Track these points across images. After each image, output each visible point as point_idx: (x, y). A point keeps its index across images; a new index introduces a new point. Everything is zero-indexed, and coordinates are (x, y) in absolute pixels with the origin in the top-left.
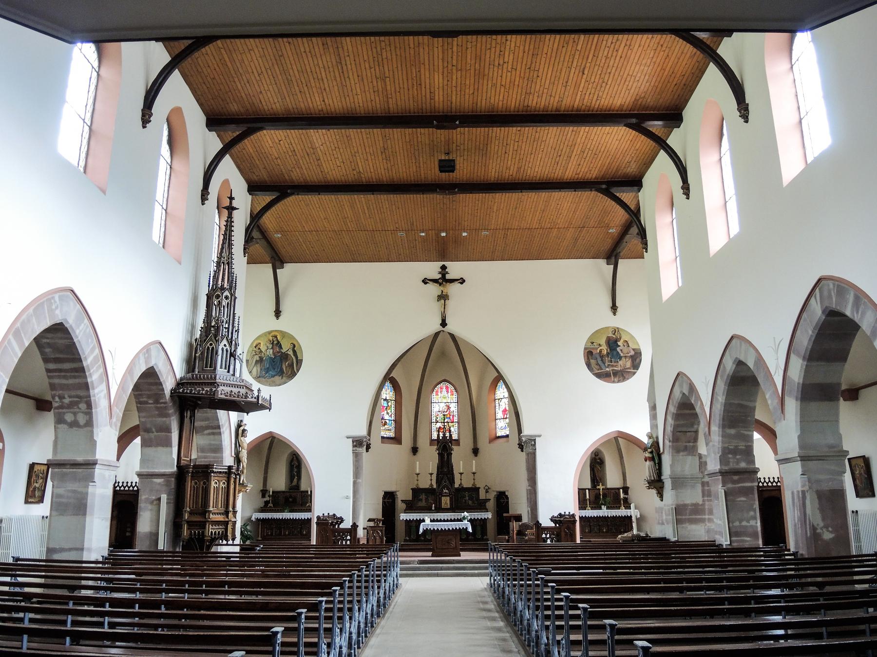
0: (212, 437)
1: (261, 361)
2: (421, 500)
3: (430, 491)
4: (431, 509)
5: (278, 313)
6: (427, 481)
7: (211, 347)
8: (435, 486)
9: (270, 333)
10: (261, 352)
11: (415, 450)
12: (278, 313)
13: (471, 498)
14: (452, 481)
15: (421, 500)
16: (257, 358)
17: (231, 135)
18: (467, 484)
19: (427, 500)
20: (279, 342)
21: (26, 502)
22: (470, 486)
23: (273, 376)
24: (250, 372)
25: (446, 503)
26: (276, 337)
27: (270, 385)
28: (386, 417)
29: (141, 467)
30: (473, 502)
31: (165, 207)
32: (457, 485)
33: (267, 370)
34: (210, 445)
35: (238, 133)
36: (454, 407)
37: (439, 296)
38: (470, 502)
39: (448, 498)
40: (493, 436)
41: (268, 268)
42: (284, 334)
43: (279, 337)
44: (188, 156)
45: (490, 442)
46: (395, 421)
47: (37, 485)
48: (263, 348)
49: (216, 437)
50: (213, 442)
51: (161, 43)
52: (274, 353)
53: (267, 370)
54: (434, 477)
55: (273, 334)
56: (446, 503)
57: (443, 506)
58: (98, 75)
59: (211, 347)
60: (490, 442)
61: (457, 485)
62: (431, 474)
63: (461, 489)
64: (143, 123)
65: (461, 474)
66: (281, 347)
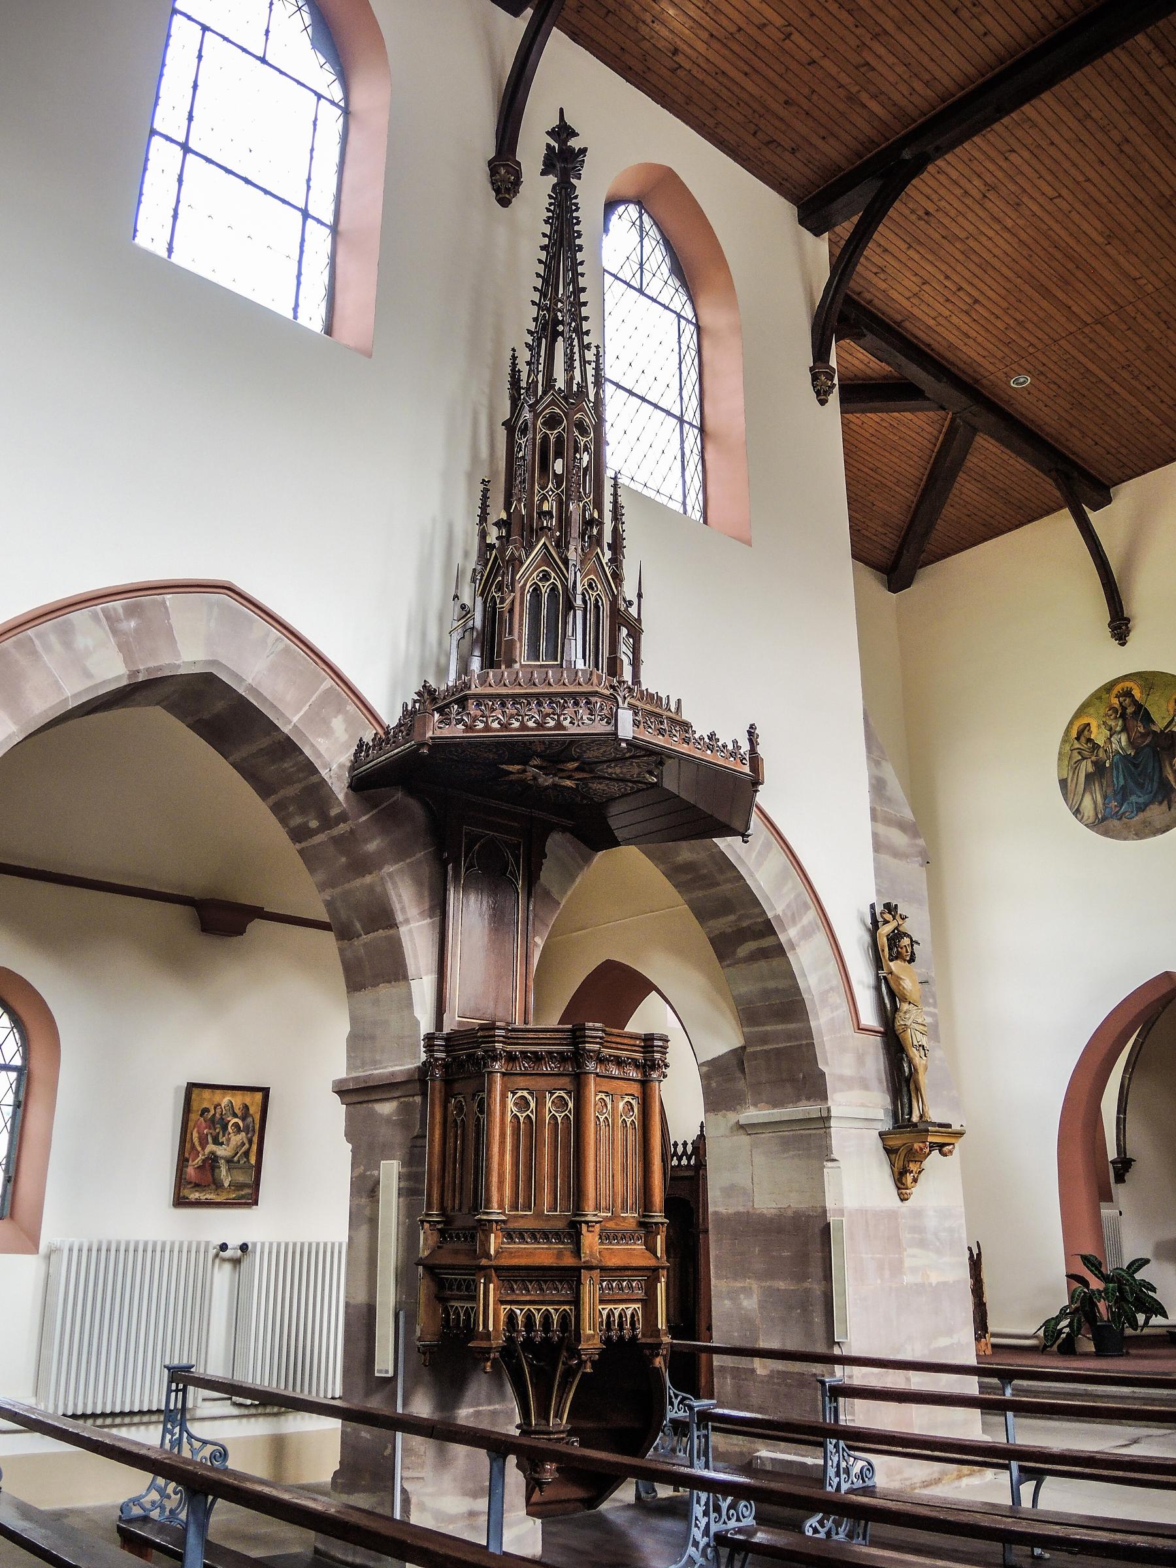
0: (762, 965)
1: (1099, 772)
5: (1120, 627)
7: (545, 588)
9: (1108, 688)
10: (1096, 747)
12: (1120, 627)
16: (1087, 767)
17: (845, 229)
20: (1139, 707)
21: (180, 1202)
23: (1141, 808)
24: (1077, 812)
26: (1128, 694)
27: (1139, 835)
29: (350, 1068)
31: (691, 415)
33: (1123, 795)
34: (766, 993)
35: (855, 219)
41: (1063, 523)
42: (1149, 680)
43: (1137, 693)
44: (386, 61)
47: (221, 1151)
48: (1099, 735)
49: (775, 962)
50: (771, 984)
52: (1131, 742)
53: (1123, 795)
55: (1118, 688)
58: (698, 327)
59: (545, 588)
64: (818, 393)
66: (1147, 719)
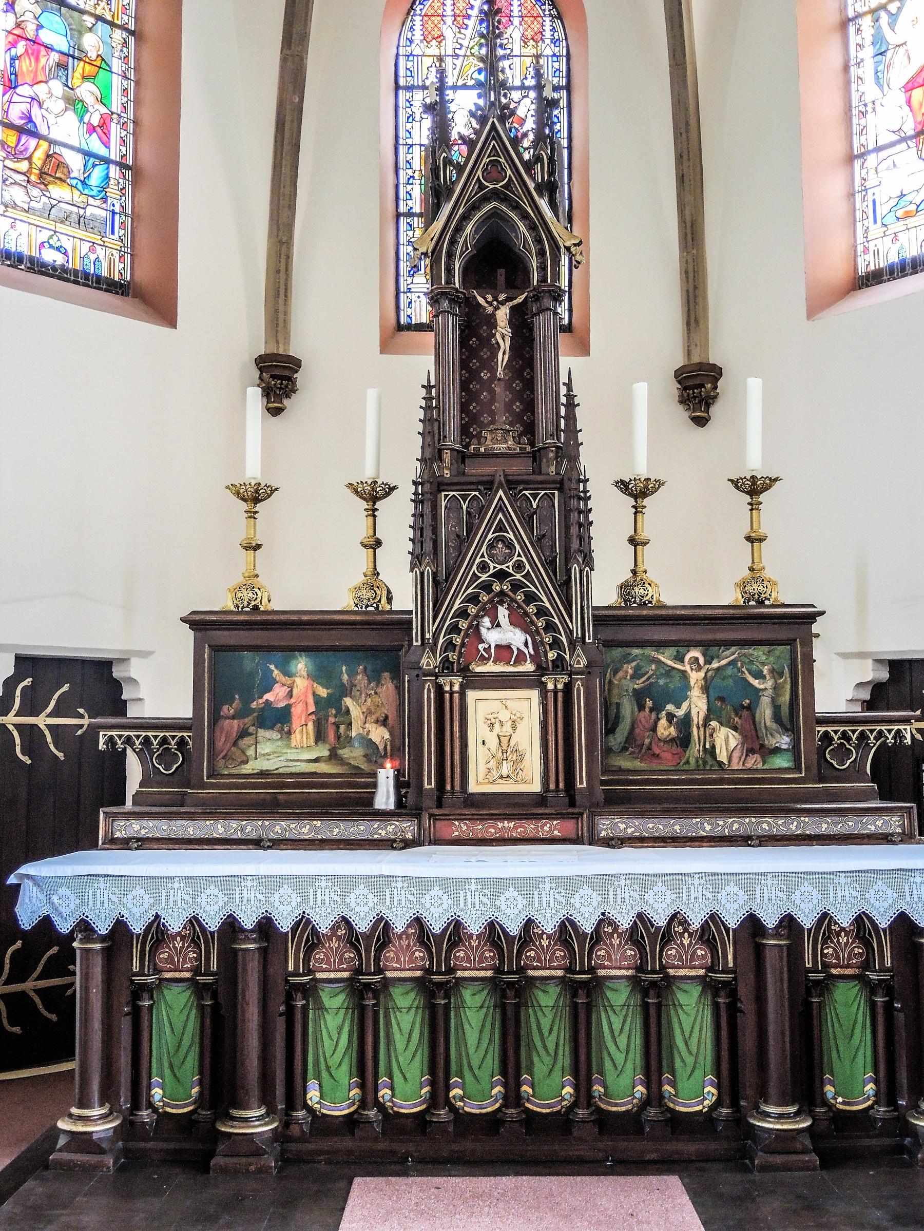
2: (278, 719)
3: (366, 641)
4: (360, 804)
6: (337, 556)
8: (404, 595)
11: (278, 377)
13: (733, 704)
14: (568, 552)
15: (278, 719)
18: (693, 572)
19: (329, 719)
22: (726, 595)
25: (507, 750)
28: (65, 128)
30: (754, 744)
32: (604, 591)
36: (776, 1205)
37: (622, 482)
38: (726, 741)
39: (526, 705)
40: (836, 270)
45: (812, 312)
46: (132, 169)
51: (674, 1181)
54: (397, 517)
56: (507, 750)
57: (481, 779)
60: (812, 312)
61: (604, 591)
62: (374, 495)
63: (636, 623)
65: (638, 491)
